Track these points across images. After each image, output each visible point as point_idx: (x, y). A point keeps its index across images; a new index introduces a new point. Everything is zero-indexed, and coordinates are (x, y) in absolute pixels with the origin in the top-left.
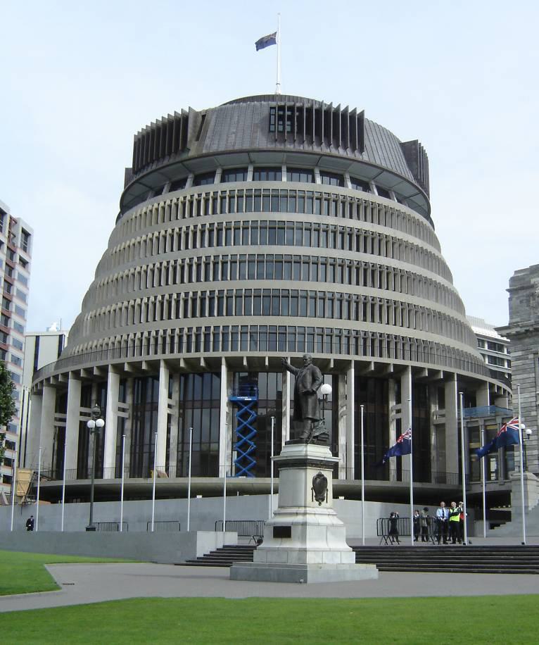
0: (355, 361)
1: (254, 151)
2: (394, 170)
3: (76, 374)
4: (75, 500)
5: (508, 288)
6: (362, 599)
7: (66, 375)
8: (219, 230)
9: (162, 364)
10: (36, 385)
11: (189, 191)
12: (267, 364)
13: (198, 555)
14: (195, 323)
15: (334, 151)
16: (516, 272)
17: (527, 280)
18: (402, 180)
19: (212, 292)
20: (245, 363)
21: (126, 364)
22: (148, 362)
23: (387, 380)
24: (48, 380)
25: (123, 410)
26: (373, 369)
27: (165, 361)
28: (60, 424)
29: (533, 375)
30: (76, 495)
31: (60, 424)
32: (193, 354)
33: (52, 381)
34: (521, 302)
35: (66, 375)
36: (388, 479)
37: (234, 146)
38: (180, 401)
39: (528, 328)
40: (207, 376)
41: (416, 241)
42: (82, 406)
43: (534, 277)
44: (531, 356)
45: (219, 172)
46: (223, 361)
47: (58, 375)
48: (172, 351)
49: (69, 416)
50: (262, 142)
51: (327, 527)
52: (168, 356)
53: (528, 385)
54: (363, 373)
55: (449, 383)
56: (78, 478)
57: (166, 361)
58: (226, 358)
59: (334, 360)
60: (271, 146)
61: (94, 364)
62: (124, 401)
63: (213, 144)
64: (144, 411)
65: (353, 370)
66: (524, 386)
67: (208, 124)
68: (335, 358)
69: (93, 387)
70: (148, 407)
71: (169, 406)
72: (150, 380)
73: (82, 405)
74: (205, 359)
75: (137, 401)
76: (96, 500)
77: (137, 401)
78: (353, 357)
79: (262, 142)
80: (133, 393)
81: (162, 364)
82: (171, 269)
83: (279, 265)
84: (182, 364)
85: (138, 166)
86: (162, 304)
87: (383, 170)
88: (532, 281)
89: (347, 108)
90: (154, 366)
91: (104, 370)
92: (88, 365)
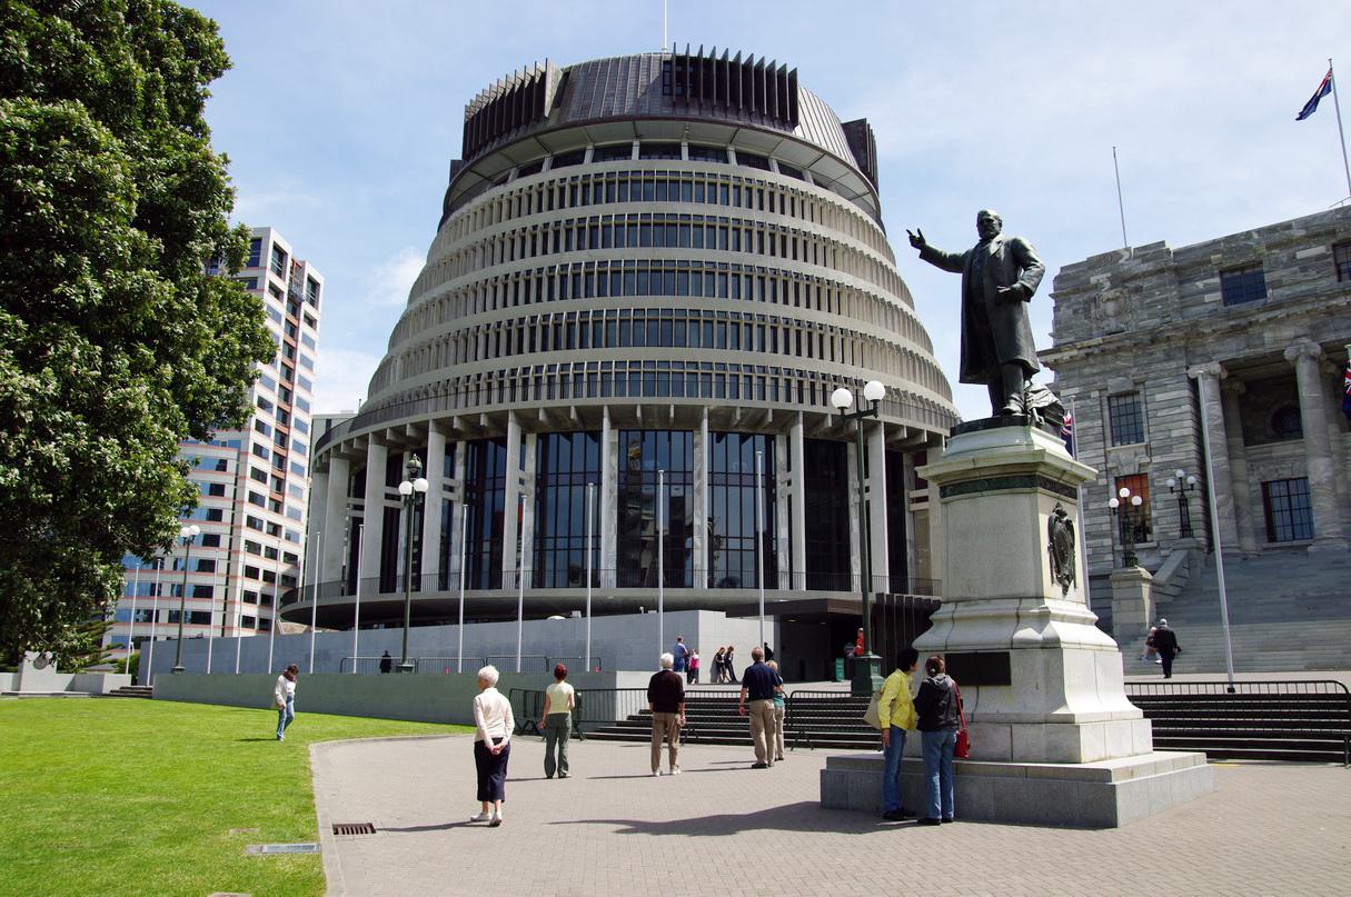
1: (642, 118)
2: (837, 155)
4: (375, 626)
5: (1052, 292)
7: (364, 439)
10: (320, 457)
11: (548, 175)
12: (672, 415)
16: (1062, 269)
17: (1083, 278)
18: (848, 170)
20: (639, 414)
22: (490, 415)
23: (845, 445)
24: (337, 447)
25: (451, 489)
26: (830, 424)
28: (357, 514)
30: (376, 616)
31: (357, 514)
32: (557, 402)
34: (1075, 312)
35: (364, 439)
36: (848, 588)
38: (537, 475)
39: (1089, 351)
40: (578, 438)
41: (874, 254)
43: (1097, 274)
47: (353, 439)
48: (525, 398)
49: (367, 501)
52: (520, 404)
53: (1091, 438)
54: (818, 433)
55: (934, 449)
56: (382, 591)
57: (518, 413)
58: (609, 406)
60: (667, 112)
62: (452, 475)
64: (483, 493)
65: (801, 426)
66: (1085, 439)
67: (571, 94)
70: (489, 484)
72: (491, 445)
73: (388, 484)
74: (578, 409)
75: (472, 476)
77: (472, 476)
80: (466, 464)
81: (511, 417)
84: (542, 416)
85: (471, 146)
87: (825, 153)
88: (1093, 280)
89: (773, 63)
90: (499, 421)
92: (397, 422)
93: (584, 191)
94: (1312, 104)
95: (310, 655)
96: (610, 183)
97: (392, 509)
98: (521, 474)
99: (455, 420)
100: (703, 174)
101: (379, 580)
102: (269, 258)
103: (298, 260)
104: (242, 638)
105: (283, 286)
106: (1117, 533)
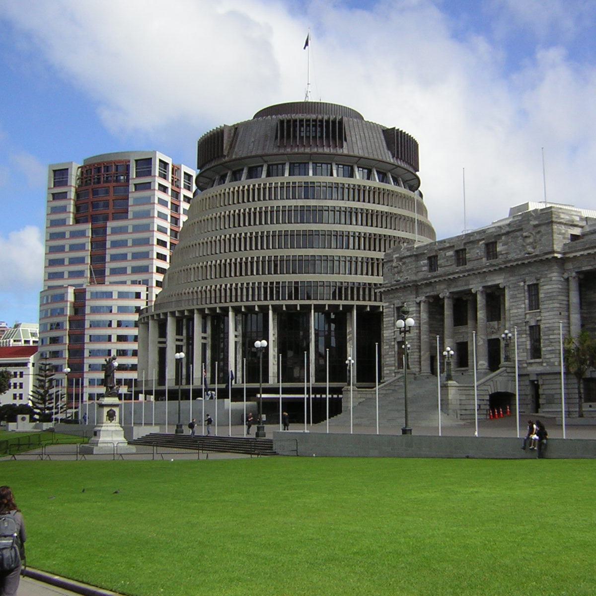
0: (357, 305)
3: (173, 313)
8: (278, 211)
9: (230, 308)
13: (134, 438)
14: (240, 280)
15: (320, 150)
19: (264, 257)
22: (221, 308)
27: (232, 307)
28: (161, 345)
30: (173, 395)
35: (165, 314)
42: (177, 335)
44: (392, 306)
45: (245, 171)
50: (271, 149)
51: (112, 431)
59: (300, 305)
60: (275, 151)
61: (185, 307)
63: (240, 152)
65: (355, 312)
67: (238, 135)
68: (315, 303)
69: (184, 322)
71: (236, 336)
78: (355, 303)
79: (271, 149)
81: (230, 308)
83: (308, 239)
86: (235, 264)
91: (192, 312)
93: (269, 191)
95: (243, 414)
98: (237, 333)
100: (314, 183)
101: (174, 380)
102: (157, 169)
103: (176, 164)
104: (263, 388)
105: (168, 184)
106: (396, 364)
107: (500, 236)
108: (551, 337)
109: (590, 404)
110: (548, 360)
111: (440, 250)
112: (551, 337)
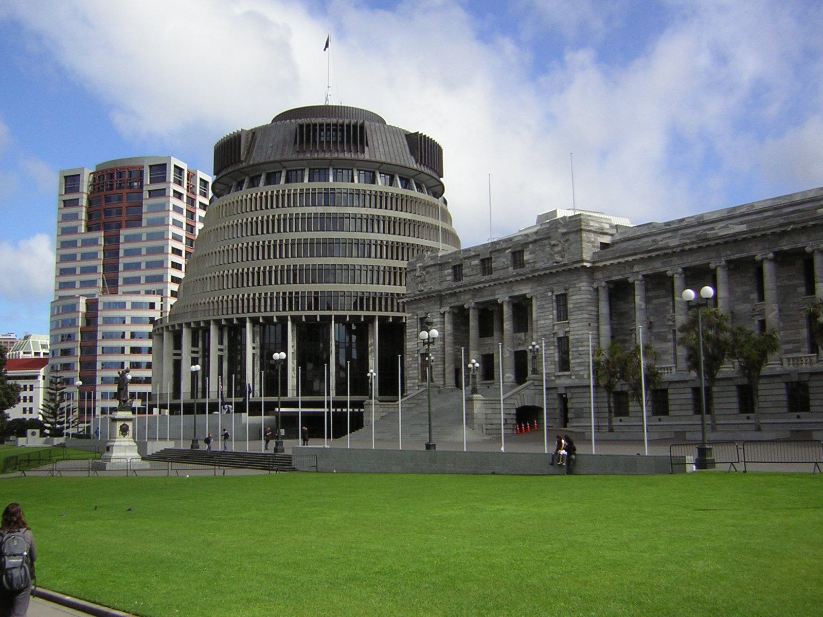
3: (188, 325)
6: (443, 472)
9: (248, 319)
19: (282, 267)
21: (192, 323)
24: (167, 327)
27: (250, 318)
29: (416, 330)
30: (189, 409)
33: (170, 329)
35: (181, 325)
37: (269, 158)
42: (192, 346)
45: (263, 177)
46: (289, 318)
50: (290, 154)
60: (294, 156)
61: (201, 318)
69: (200, 334)
71: (254, 348)
76: (197, 414)
79: (290, 154)
81: (248, 319)
82: (255, 248)
83: (328, 247)
91: (208, 323)
94: (327, 45)
95: (261, 429)
96: (305, 244)
97: (194, 358)
98: (254, 345)
99: (223, 321)
106: (420, 377)
107: (527, 244)
108: (580, 349)
109: (659, 417)
110: (576, 373)
111: (465, 258)
112: (580, 349)
